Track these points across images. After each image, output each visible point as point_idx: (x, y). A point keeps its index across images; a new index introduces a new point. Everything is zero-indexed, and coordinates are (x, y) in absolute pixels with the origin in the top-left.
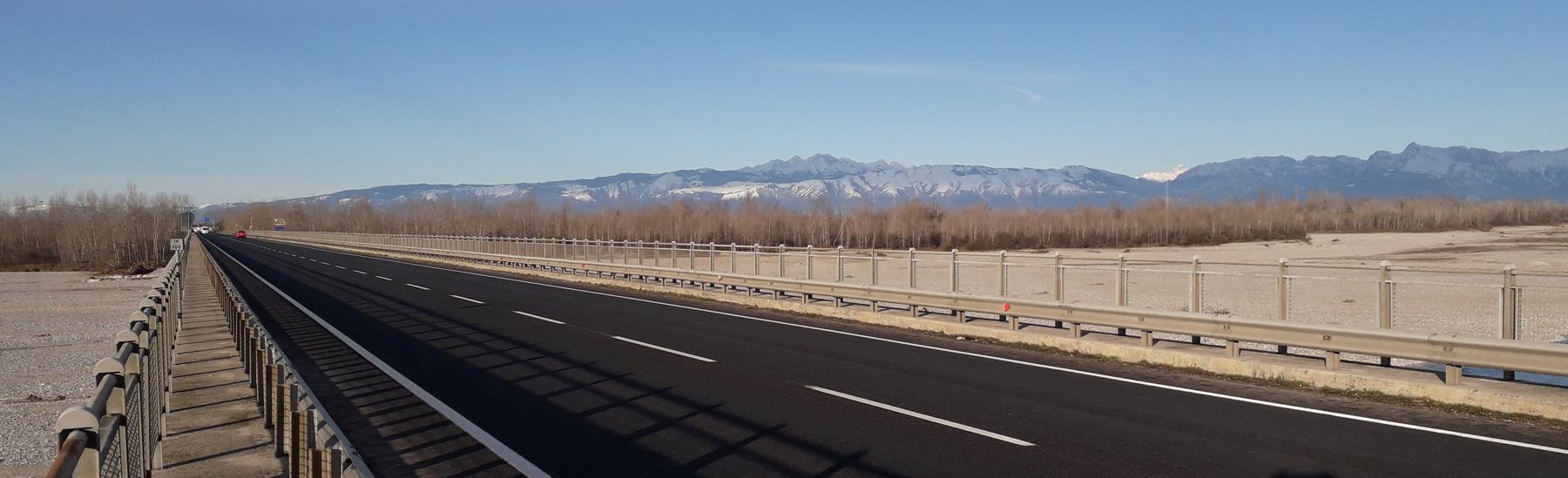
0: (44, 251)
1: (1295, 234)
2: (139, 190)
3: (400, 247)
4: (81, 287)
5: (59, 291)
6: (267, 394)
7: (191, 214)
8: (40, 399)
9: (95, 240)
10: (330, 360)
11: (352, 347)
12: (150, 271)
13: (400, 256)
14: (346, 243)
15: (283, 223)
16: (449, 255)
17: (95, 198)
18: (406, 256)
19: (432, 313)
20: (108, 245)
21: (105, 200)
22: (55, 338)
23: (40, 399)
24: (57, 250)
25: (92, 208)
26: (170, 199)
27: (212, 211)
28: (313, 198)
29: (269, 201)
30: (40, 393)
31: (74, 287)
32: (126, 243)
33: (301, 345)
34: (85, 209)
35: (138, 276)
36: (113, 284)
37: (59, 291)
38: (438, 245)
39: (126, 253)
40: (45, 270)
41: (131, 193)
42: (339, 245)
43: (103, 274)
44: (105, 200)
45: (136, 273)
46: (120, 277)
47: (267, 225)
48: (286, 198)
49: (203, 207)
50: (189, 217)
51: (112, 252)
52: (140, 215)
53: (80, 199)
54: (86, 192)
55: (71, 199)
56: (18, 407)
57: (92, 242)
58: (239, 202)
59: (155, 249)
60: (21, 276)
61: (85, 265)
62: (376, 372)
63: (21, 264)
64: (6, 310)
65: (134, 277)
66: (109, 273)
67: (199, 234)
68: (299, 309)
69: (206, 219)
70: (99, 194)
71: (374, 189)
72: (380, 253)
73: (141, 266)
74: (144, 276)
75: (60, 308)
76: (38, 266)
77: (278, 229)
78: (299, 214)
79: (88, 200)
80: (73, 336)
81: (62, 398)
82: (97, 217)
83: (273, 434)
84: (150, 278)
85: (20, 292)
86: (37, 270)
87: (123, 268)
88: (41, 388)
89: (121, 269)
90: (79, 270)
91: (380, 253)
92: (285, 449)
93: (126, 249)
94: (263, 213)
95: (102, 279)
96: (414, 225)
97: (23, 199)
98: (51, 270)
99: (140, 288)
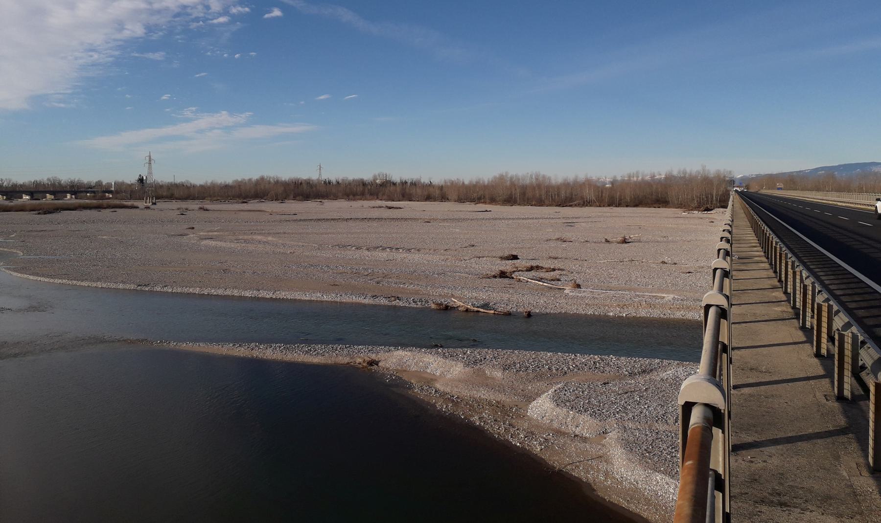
0: (662, 198)
1: (10, 211)
2: (707, 168)
3: (844, 200)
4: (679, 216)
5: (670, 217)
6: (793, 302)
7: (734, 181)
8: (666, 263)
9: (686, 193)
10: (840, 277)
11: (824, 252)
12: (711, 210)
13: (844, 204)
14: (815, 197)
15: (782, 186)
16: (871, 204)
17: (686, 173)
18: (847, 205)
19: (870, 239)
20: (692, 196)
21: (691, 173)
22: (670, 238)
23: (666, 263)
24: (668, 198)
25: (684, 177)
26: (722, 173)
27: (743, 179)
28: (800, 171)
29: (775, 173)
30: (666, 261)
31: (676, 216)
32: (700, 195)
33: (794, 249)
34: (681, 178)
35: (706, 212)
36: (694, 216)
37: (670, 217)
38: (866, 199)
39: (700, 200)
40: (662, 208)
41: (703, 170)
42: (811, 198)
43: (689, 210)
44: (691, 173)
45: (704, 211)
46: (697, 212)
47: (773, 187)
48: (784, 171)
49: (738, 177)
50: (732, 182)
51: (693, 200)
52: (707, 181)
53: (679, 172)
54: (682, 170)
55: (675, 173)
56: (657, 266)
57: (684, 195)
58: (758, 173)
59: (714, 198)
60: (652, 210)
61: (682, 205)
62: (856, 280)
63: (652, 204)
64: (647, 225)
65: (703, 212)
66: (692, 210)
67: (736, 191)
68: (799, 237)
69: (740, 184)
70: (688, 171)
71: (840, 166)
72: (834, 203)
73: (707, 207)
74: (709, 212)
75: (670, 226)
76: (660, 206)
77: (779, 189)
78: (792, 180)
79: (683, 173)
80: (678, 238)
81: (675, 264)
82: (687, 181)
83: (833, 382)
84: (711, 213)
85: (653, 217)
86: (659, 207)
87: (698, 208)
88: (666, 259)
89: (698, 208)
90: (678, 208)
91: (834, 203)
92: (845, 394)
93: (700, 198)
94: (771, 180)
95: (689, 213)
96: (862, 188)
97: (654, 173)
98: (665, 208)
99: (707, 218)
